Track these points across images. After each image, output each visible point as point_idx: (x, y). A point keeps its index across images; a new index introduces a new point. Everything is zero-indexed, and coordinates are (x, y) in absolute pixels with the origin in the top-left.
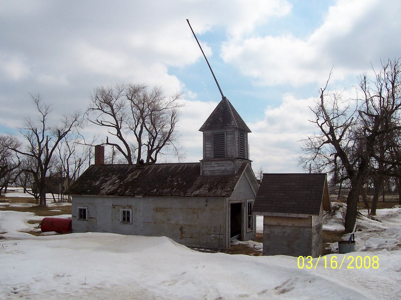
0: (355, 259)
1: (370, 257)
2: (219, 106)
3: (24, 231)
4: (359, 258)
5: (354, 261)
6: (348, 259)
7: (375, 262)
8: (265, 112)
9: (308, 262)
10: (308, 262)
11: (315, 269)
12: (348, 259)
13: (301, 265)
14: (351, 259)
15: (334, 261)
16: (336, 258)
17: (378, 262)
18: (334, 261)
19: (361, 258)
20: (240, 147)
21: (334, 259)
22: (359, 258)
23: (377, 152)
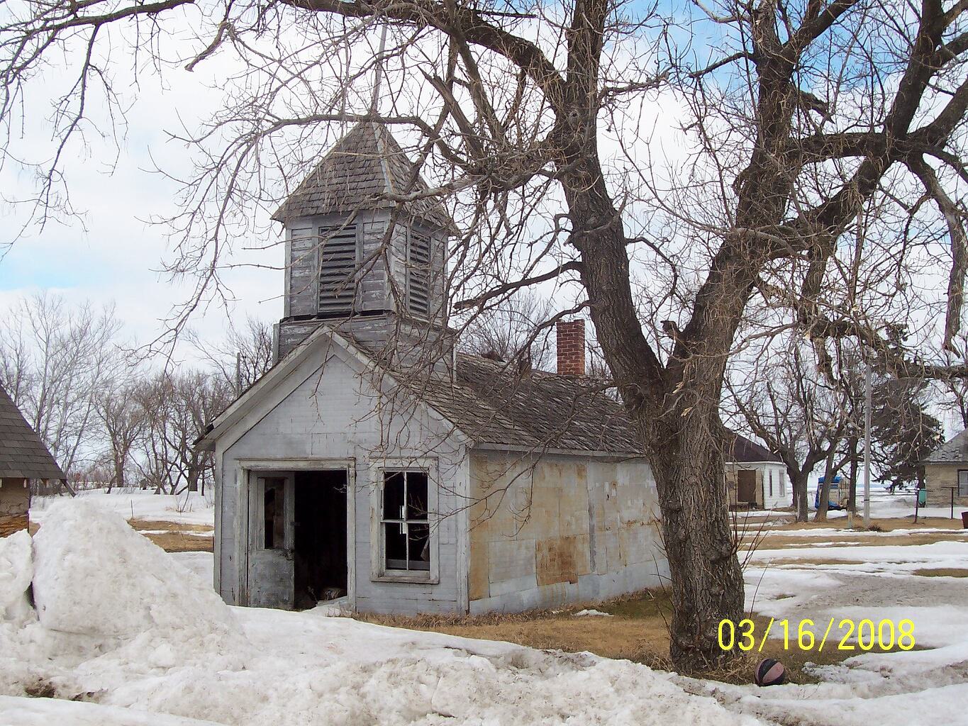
0: (857, 626)
1: (892, 621)
2: (98, 18)
3: (402, 585)
4: (726, 625)
5: (856, 631)
6: (841, 626)
7: (904, 634)
8: (962, 444)
9: (744, 634)
10: (744, 634)
11: (760, 650)
12: (841, 626)
13: (726, 642)
14: (847, 626)
15: (806, 632)
16: (811, 623)
17: (752, 634)
18: (806, 632)
19: (731, 624)
20: (411, 287)
21: (806, 627)
22: (726, 625)
23: (507, 139)
